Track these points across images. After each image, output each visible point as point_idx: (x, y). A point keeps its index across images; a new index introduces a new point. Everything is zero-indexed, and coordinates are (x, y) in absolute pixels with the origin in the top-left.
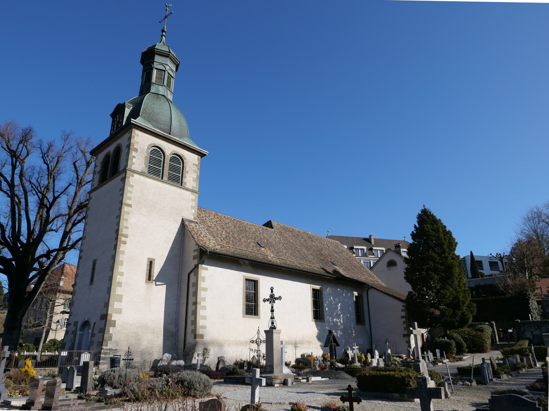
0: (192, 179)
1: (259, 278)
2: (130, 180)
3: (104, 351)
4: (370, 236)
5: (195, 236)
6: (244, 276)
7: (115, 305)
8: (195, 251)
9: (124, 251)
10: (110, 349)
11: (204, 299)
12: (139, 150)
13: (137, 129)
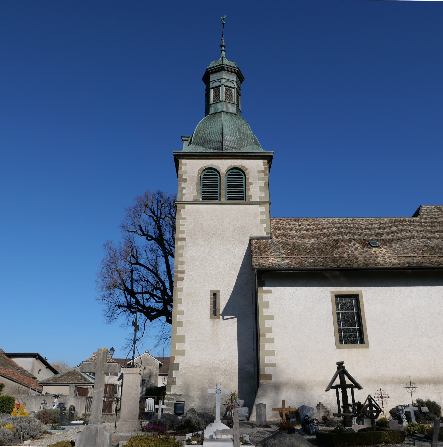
0: (258, 189)
1: (361, 291)
2: (181, 212)
3: (167, 397)
6: (332, 292)
7: (177, 346)
9: (182, 289)
10: (174, 395)
11: (270, 330)
12: (188, 179)
13: (183, 158)
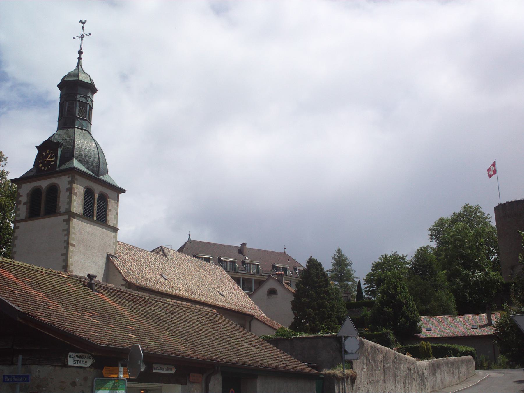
2: (73, 222)
12: (78, 193)
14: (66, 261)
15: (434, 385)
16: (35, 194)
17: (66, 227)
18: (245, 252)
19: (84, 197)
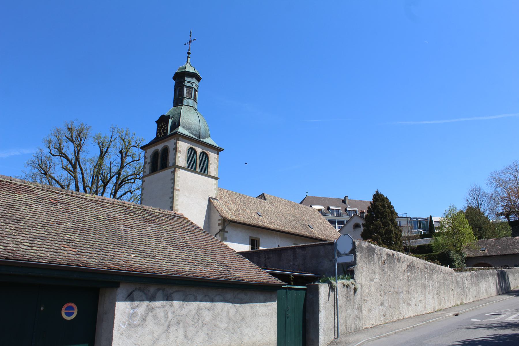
2: (178, 173)
4: (345, 197)
5: (219, 210)
8: (219, 220)
12: (182, 151)
14: (172, 202)
15: (477, 295)
16: (155, 155)
17: (173, 177)
18: (347, 202)
19: (187, 154)
